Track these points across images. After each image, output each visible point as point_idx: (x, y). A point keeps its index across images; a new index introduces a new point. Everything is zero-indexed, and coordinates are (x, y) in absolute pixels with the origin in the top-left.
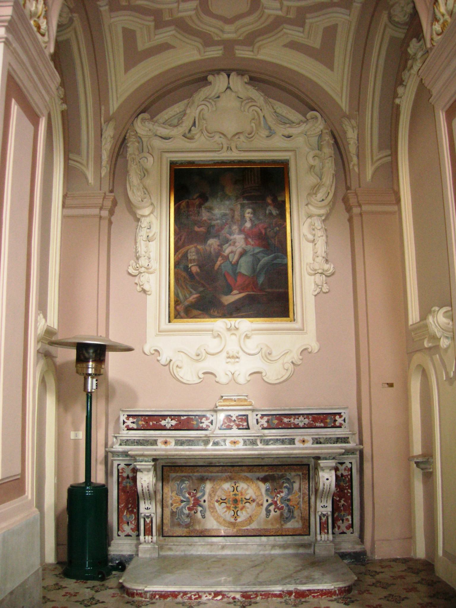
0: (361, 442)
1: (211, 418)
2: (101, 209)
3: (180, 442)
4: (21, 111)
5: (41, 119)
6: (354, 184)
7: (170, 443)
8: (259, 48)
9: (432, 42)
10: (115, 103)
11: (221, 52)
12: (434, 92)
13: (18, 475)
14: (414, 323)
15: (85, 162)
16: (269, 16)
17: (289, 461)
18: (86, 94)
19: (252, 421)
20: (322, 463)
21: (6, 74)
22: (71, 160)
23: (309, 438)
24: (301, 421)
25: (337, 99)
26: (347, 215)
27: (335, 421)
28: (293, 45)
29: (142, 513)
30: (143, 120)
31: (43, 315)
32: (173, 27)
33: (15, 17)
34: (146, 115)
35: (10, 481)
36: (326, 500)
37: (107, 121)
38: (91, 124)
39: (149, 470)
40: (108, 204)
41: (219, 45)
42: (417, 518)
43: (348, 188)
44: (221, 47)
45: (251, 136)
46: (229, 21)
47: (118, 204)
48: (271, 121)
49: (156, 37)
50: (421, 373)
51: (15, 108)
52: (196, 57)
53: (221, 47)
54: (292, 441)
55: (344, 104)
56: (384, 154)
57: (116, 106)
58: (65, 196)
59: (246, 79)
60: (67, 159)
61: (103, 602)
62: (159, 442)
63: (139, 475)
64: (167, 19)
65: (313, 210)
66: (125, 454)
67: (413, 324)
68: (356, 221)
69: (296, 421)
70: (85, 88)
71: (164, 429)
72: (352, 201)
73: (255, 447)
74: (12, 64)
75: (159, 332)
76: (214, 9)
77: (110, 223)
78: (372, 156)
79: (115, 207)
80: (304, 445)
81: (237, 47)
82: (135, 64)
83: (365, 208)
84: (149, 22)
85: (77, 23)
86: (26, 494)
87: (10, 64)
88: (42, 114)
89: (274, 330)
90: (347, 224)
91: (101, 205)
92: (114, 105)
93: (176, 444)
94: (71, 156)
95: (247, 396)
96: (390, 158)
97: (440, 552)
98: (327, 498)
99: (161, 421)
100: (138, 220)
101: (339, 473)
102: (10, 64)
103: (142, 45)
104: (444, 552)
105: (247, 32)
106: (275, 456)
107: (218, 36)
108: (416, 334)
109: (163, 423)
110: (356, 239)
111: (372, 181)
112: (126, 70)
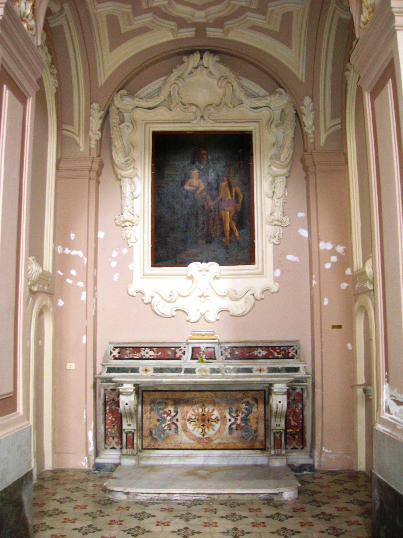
1: (184, 350)
3: (158, 370)
4: (14, 98)
5: (28, 99)
6: (310, 148)
8: (228, 30)
11: (194, 33)
13: (10, 393)
14: (358, 269)
15: (76, 132)
16: (234, 5)
24: (147, 353)
25: (296, 73)
26: (304, 174)
27: (176, 353)
28: (254, 28)
30: (122, 96)
32: (151, 14)
34: (123, 92)
35: (4, 399)
36: (279, 420)
40: (96, 166)
41: (192, 27)
43: (305, 151)
44: (194, 29)
45: (217, 108)
46: (179, 86)
47: (105, 166)
49: (136, 22)
50: (364, 313)
53: (194, 29)
54: (249, 370)
55: (301, 74)
56: (336, 123)
57: (103, 82)
58: (58, 161)
60: (60, 129)
61: (154, 516)
62: (140, 370)
65: (276, 170)
67: (358, 270)
68: (312, 177)
69: (151, 353)
70: (77, 66)
71: (256, 358)
72: (309, 162)
73: (193, 375)
75: (144, 275)
77: (98, 182)
78: (325, 124)
79: (102, 169)
80: (260, 373)
82: (120, 44)
86: (18, 411)
89: (239, 275)
90: (305, 182)
91: (90, 168)
92: (102, 80)
94: (64, 127)
95: (213, 332)
96: (340, 126)
98: (281, 418)
100: (120, 180)
106: (255, 383)
107: (190, 20)
108: (360, 279)
109: (256, 353)
110: (312, 211)
111: (325, 145)
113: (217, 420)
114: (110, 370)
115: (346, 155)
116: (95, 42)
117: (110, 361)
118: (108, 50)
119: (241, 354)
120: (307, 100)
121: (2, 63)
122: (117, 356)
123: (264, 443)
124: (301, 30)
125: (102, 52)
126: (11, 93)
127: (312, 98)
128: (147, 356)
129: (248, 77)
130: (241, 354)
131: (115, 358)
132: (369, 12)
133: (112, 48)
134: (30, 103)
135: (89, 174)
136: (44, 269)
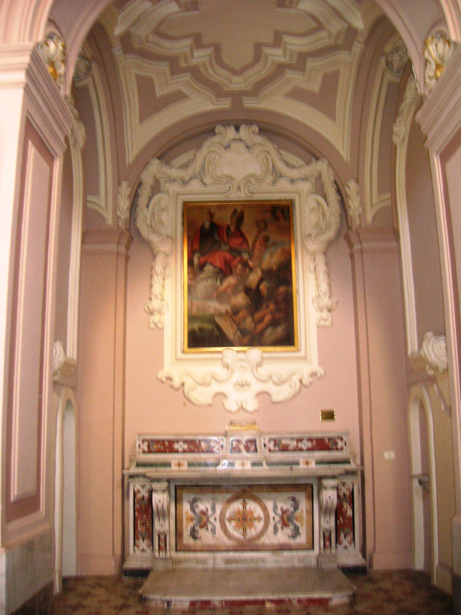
0: (362, 464)
4: (37, 152)
7: (183, 465)
10: (130, 155)
12: (429, 138)
18: (105, 164)
19: (259, 445)
20: (326, 482)
21: (25, 119)
26: (347, 250)
32: (188, 74)
33: (33, 66)
38: (107, 133)
40: (125, 241)
42: (416, 531)
48: (280, 166)
51: (32, 150)
52: (210, 107)
59: (256, 128)
63: (155, 496)
68: (357, 257)
72: (353, 238)
74: (30, 111)
76: (226, 60)
77: (127, 258)
81: (244, 98)
83: (365, 245)
84: (165, 67)
85: (95, 72)
87: (28, 112)
88: (56, 155)
92: (130, 158)
97: (436, 562)
102: (28, 112)
103: (160, 92)
104: (440, 563)
107: (227, 86)
110: (357, 272)
114: (139, 465)
116: (124, 110)
118: (137, 120)
119: (274, 594)
120: (352, 184)
121: (27, 116)
123: (319, 291)
124: (343, 140)
125: (131, 130)
126: (36, 150)
127: (357, 182)
129: (286, 150)
131: (144, 452)
133: (143, 117)
135: (117, 248)
136: (68, 355)
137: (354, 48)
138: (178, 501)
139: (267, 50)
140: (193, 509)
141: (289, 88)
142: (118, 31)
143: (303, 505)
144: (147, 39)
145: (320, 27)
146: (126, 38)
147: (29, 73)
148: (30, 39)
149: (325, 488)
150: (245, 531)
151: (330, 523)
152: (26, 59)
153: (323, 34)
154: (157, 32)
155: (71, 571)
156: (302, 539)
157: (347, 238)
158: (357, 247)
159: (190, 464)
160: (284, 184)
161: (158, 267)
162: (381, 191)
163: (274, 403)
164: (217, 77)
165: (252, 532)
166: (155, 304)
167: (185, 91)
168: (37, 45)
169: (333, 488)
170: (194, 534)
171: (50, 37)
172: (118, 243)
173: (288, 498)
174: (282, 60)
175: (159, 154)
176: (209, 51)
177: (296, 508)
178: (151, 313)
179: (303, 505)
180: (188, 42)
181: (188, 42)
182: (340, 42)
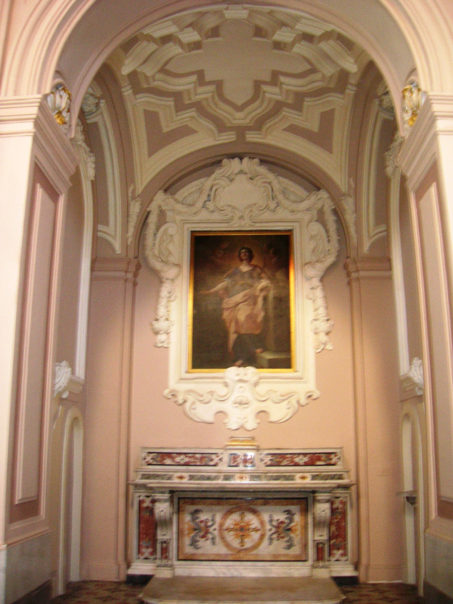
2: (126, 272)
4: (47, 197)
5: (61, 197)
6: (353, 254)
9: (204, 401)
17: (278, 490)
22: (100, 231)
23: (308, 475)
24: (301, 460)
26: (346, 280)
29: (159, 539)
31: (303, 578)
33: (40, 115)
37: (133, 198)
39: (165, 501)
40: (132, 268)
41: (232, 130)
46: (240, 109)
51: (40, 191)
59: (256, 160)
64: (187, 102)
66: (144, 486)
68: (354, 284)
72: (351, 267)
77: (135, 284)
83: (362, 273)
84: (170, 102)
92: (140, 188)
93: (190, 479)
99: (286, 518)
101: (335, 506)
105: (255, 119)
112: (150, 155)
113: (256, 530)
115: (389, 260)
117: (143, 467)
118: (146, 153)
122: (332, 456)
128: (301, 457)
130: (411, 128)
132: (284, 459)
133: (153, 150)
134: (62, 201)
137: (348, 91)
138: (179, 511)
139: (265, 88)
140: (194, 519)
141: (287, 124)
142: (126, 70)
143: (297, 518)
144: (153, 76)
145: (313, 70)
146: (133, 76)
147: (37, 123)
148: (39, 92)
149: (319, 501)
150: (242, 543)
151: (322, 536)
152: (34, 111)
153: (318, 76)
154: (163, 70)
155: (75, 577)
156: (296, 550)
157: (346, 267)
158: (354, 275)
159: (191, 478)
160: (282, 214)
161: (164, 292)
162: (378, 223)
163: (271, 422)
164: (220, 111)
165: (248, 543)
166: (161, 325)
167: (192, 125)
168: (46, 96)
169: (328, 501)
170: (194, 543)
171: (57, 87)
172: (126, 272)
173: (285, 511)
174: (279, 98)
175: (165, 187)
176: (212, 88)
177: (291, 520)
178: (157, 333)
179: (297, 518)
180: (194, 78)
181: (194, 78)
182: (332, 86)
